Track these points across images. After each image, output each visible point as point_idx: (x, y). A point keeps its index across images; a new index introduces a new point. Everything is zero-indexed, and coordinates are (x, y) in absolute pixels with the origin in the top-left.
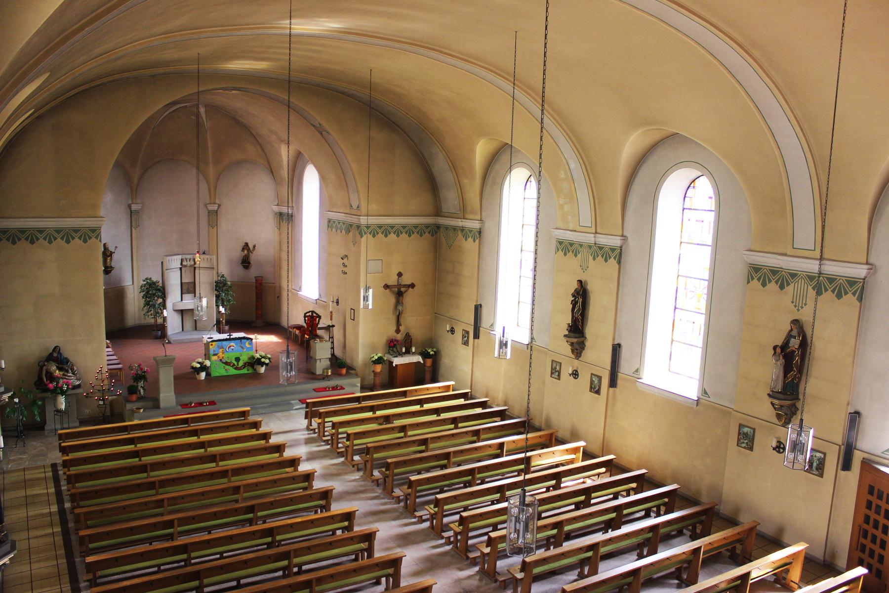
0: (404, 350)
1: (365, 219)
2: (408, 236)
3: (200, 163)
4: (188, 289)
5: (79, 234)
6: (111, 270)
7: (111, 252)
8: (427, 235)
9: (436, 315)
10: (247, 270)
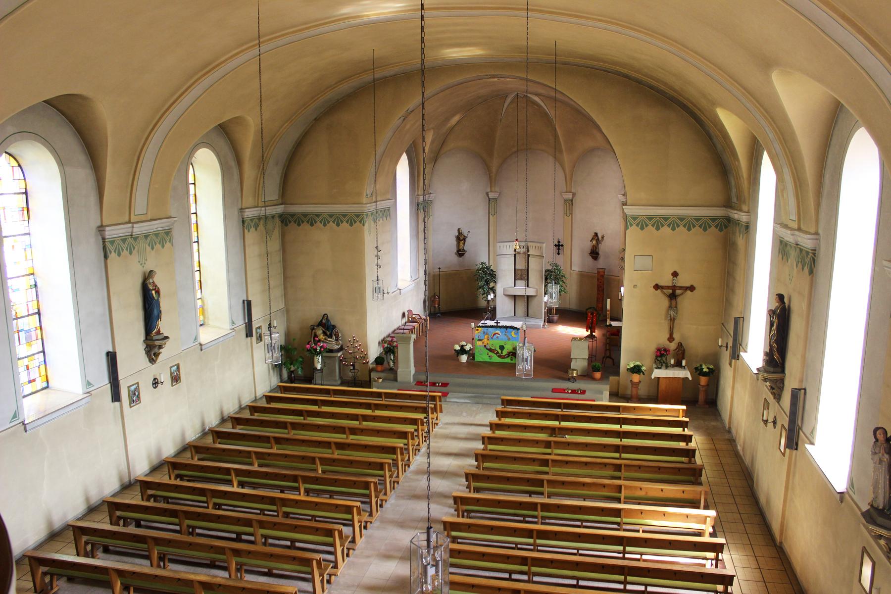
0: (672, 362)
2: (336, 225)
3: (556, 152)
4: (521, 275)
5: (346, 219)
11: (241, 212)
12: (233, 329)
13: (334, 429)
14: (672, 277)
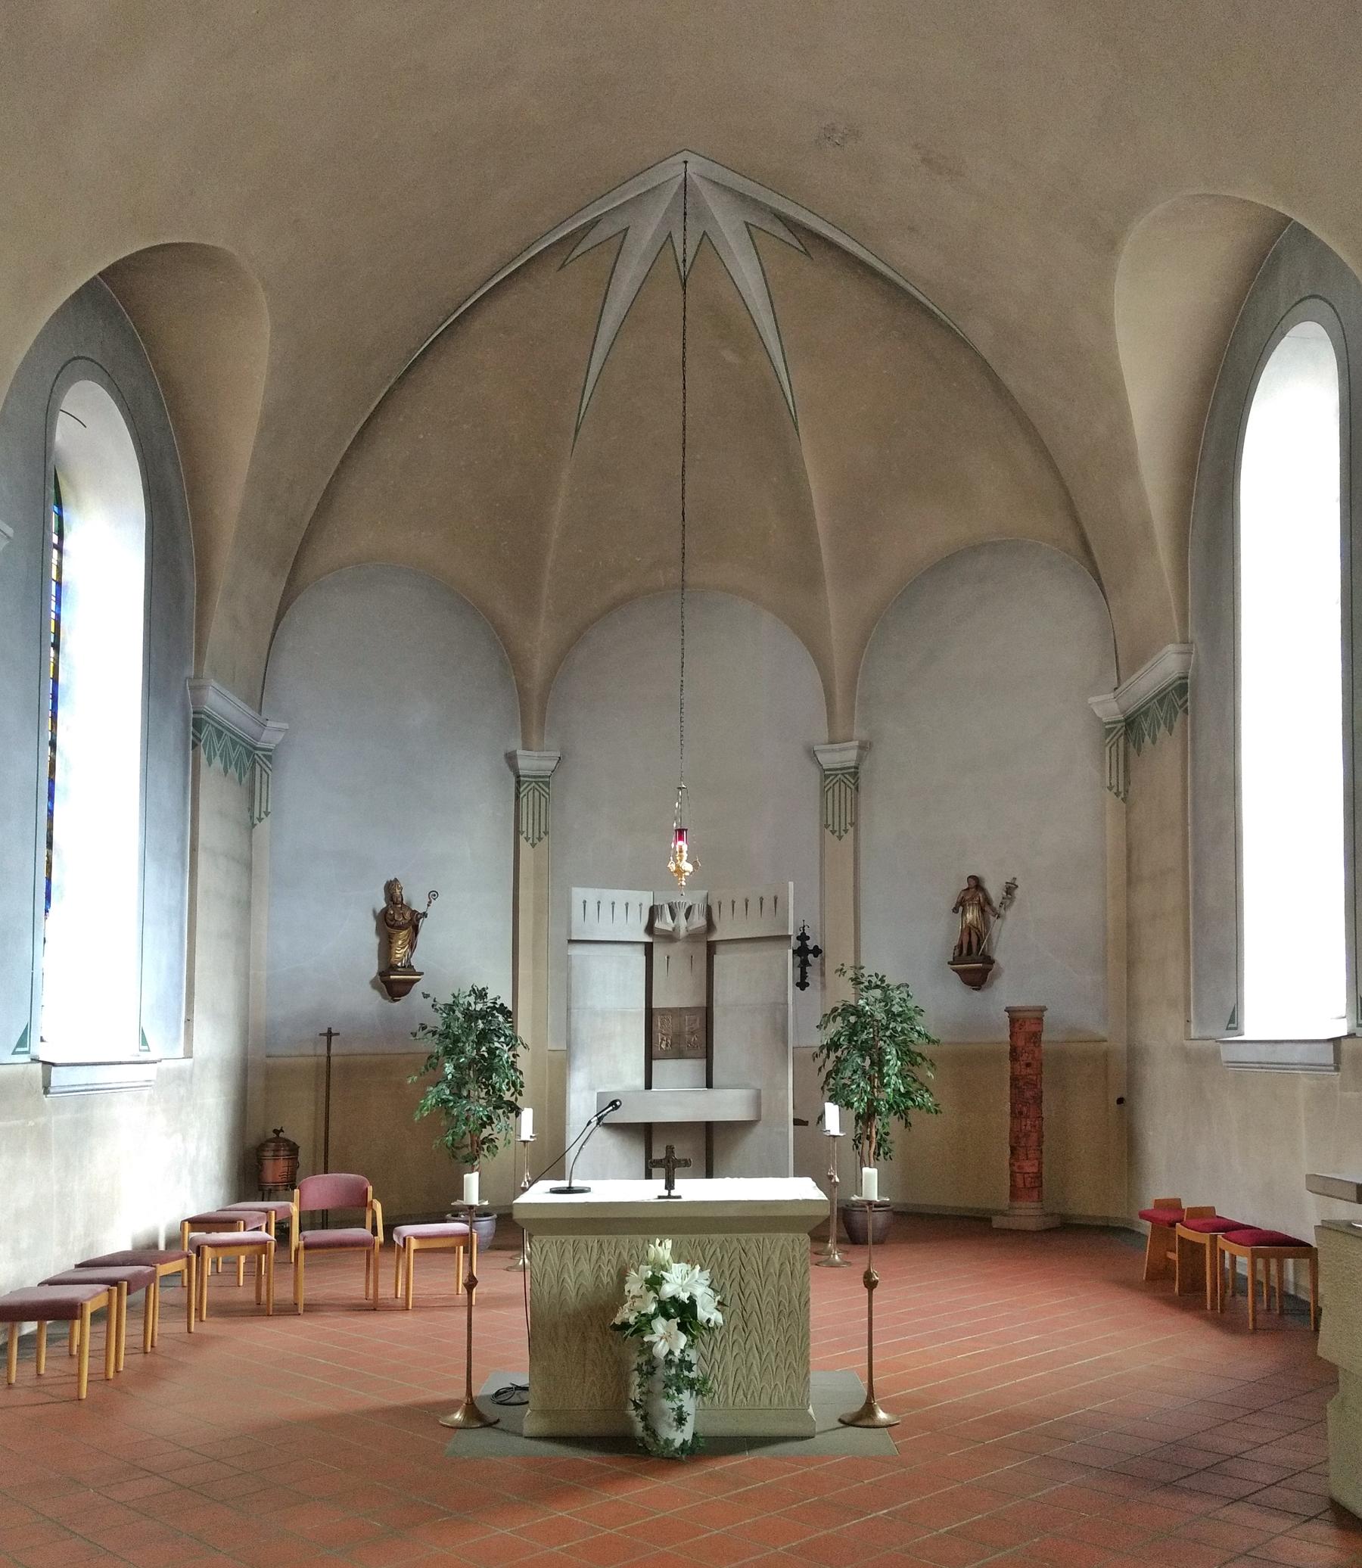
4: (678, 1036)
6: (414, 982)
10: (977, 993)
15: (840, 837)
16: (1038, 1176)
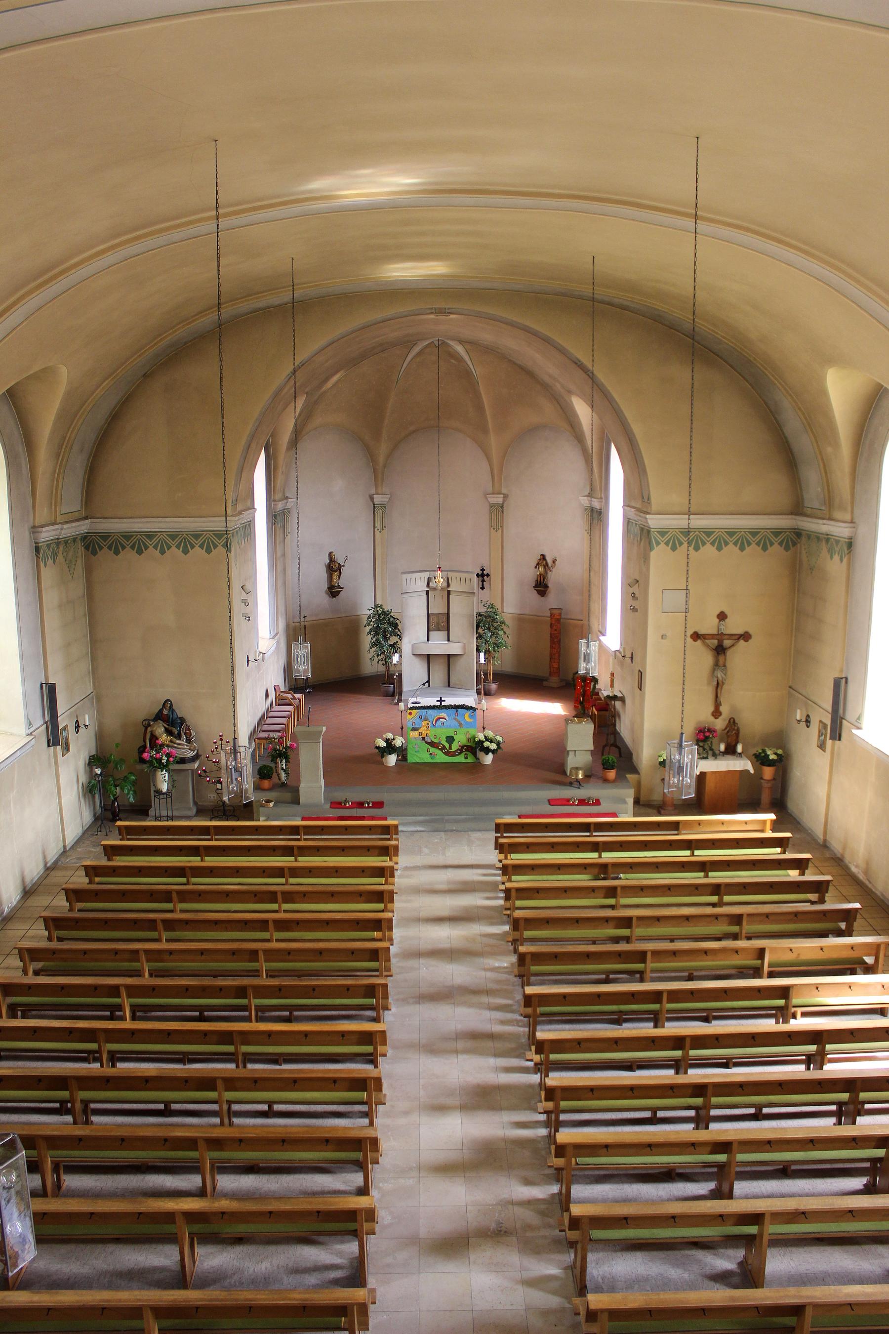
0: (722, 747)
1: (221, 521)
4: (438, 624)
5: (200, 541)
7: (339, 564)
8: (776, 549)
9: (791, 690)
11: (33, 532)
12: (31, 734)
13: (255, 895)
14: (718, 620)
15: (496, 531)
16: (558, 669)
